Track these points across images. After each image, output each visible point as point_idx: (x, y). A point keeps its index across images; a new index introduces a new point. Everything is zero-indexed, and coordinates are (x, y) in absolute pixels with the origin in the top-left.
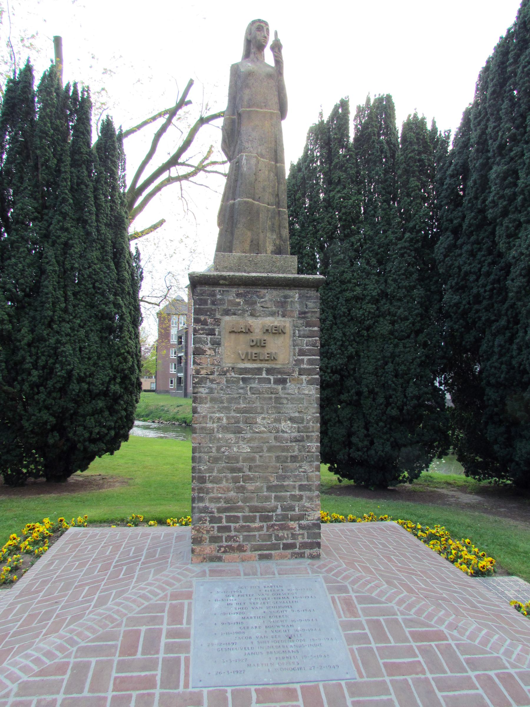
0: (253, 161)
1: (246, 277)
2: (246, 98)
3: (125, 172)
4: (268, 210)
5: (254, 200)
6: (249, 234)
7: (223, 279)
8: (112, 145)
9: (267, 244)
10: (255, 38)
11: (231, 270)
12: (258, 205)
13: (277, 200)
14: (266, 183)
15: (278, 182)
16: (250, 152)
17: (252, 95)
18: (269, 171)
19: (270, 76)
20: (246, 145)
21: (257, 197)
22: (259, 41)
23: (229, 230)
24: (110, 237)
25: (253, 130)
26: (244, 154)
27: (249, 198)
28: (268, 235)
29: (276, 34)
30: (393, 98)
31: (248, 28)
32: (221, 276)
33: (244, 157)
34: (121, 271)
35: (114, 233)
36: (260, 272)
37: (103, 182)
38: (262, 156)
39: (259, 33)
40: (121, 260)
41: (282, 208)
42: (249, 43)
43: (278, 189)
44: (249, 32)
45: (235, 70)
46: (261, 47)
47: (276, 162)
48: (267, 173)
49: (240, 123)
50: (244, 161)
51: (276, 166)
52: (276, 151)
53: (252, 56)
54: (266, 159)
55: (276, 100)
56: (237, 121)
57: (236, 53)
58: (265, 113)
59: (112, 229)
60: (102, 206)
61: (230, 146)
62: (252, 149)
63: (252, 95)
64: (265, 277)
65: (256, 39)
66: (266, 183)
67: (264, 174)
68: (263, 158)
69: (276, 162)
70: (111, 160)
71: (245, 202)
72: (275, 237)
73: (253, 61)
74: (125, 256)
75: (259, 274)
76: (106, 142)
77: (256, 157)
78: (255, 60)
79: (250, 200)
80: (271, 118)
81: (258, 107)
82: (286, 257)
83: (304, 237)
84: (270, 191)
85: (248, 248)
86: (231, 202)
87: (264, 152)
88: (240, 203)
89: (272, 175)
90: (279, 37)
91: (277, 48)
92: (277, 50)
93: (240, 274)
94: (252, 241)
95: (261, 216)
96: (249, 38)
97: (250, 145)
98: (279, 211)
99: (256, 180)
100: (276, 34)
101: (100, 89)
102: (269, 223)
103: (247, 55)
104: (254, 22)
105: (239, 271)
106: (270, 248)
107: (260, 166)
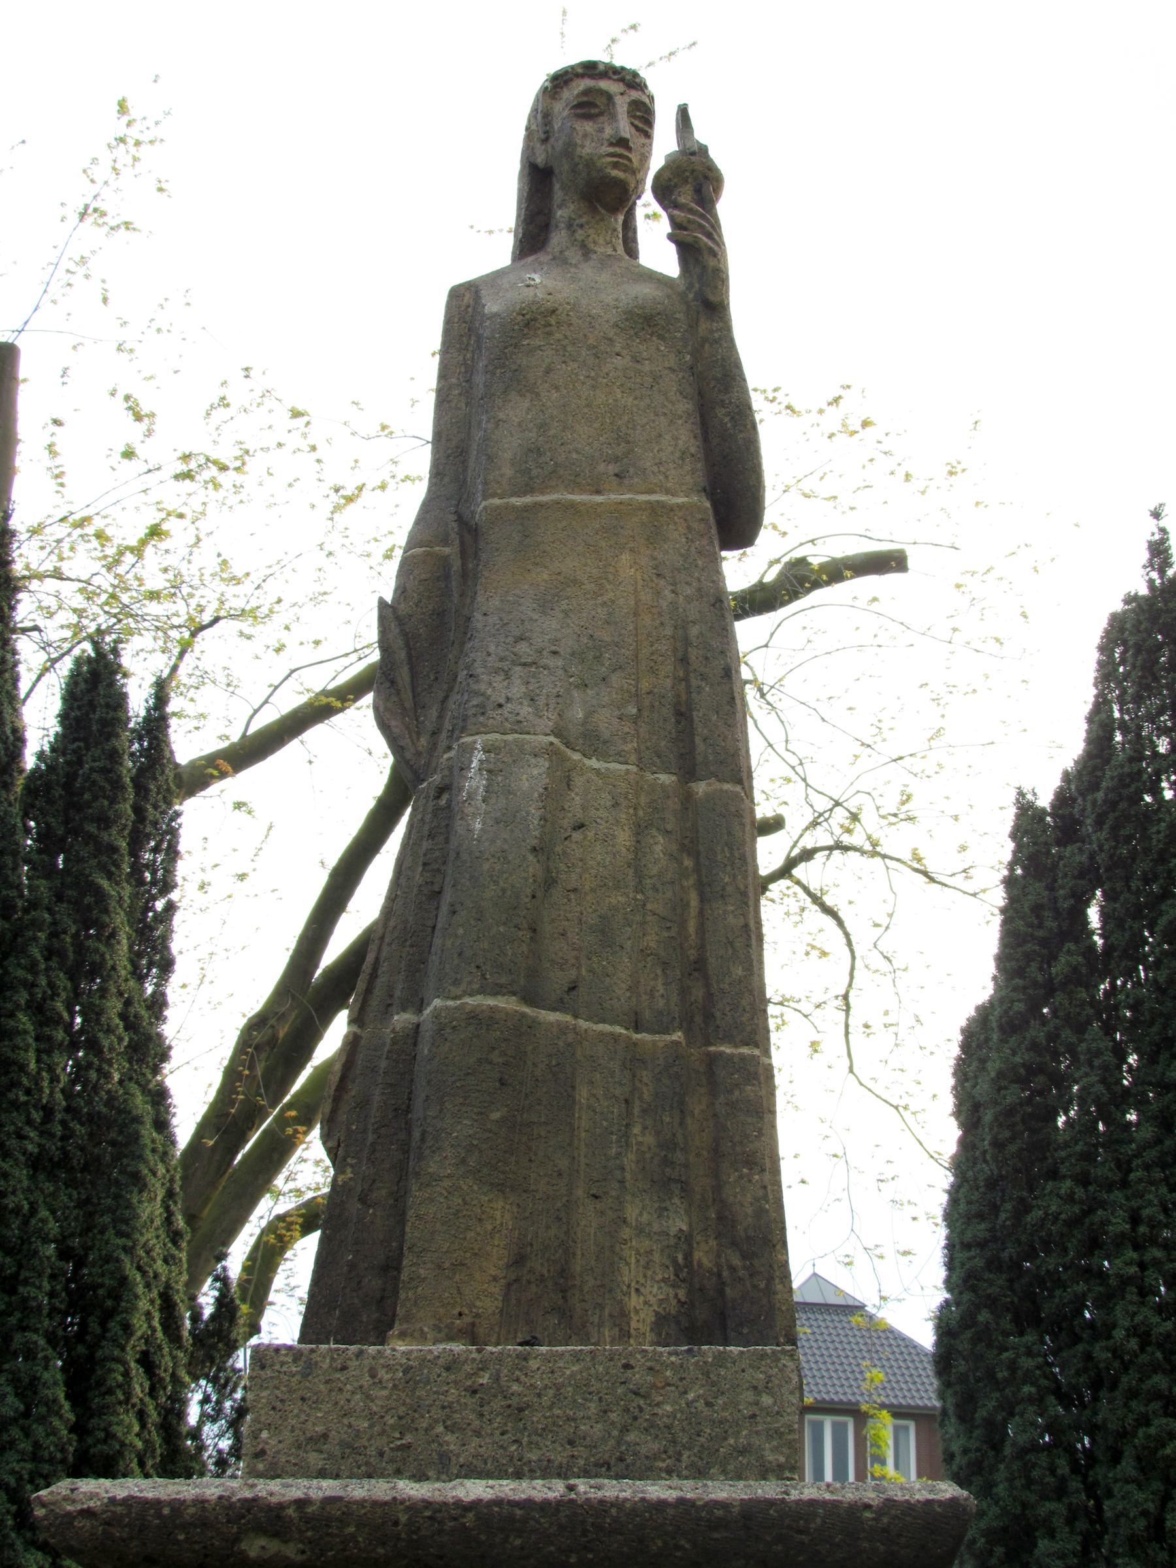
0: (532, 776)
1: (416, 1508)
2: (509, 445)
3: (174, 896)
4: (634, 1059)
5: (530, 999)
6: (501, 1211)
7: (260, 1529)
8: (105, 771)
9: (628, 1274)
10: (569, 151)
11: (352, 1459)
12: (563, 1029)
13: (698, 993)
14: (617, 899)
15: (701, 886)
16: (519, 726)
17: (543, 427)
18: (639, 830)
19: (644, 322)
20: (496, 688)
21: (558, 980)
22: (590, 163)
23: (381, 1193)
24: (53, 1227)
25: (545, 605)
26: (480, 741)
27: (497, 990)
28: (631, 1212)
29: (683, 114)
30: (712, 154)
31: (535, 110)
32: (251, 1504)
33: (478, 756)
34: (103, 1410)
35: (80, 1204)
36: (547, 1471)
37: (36, 952)
38: (593, 743)
39: (588, 126)
40: (107, 1349)
41: (728, 1039)
42: (538, 180)
43: (701, 929)
44: (541, 126)
45: (469, 319)
46: (610, 197)
47: (689, 771)
48: (624, 837)
49: (469, 577)
50: (474, 781)
51: (688, 798)
52: (683, 714)
53: (558, 238)
54: (621, 757)
55: (685, 437)
56: (456, 565)
57: (481, 235)
58: (620, 511)
59: (71, 1183)
60: (22, 1068)
61: (419, 705)
62: (526, 710)
63: (543, 427)
64: (545, 1506)
65: (589, 151)
66: (617, 899)
67: (606, 843)
68: (603, 756)
69: (689, 771)
70: (90, 838)
71: (474, 1017)
72: (678, 1223)
73: (561, 260)
74: (127, 1328)
75: (507, 1489)
76: (80, 763)
77: (551, 752)
78: (574, 255)
79: (507, 1004)
80: (654, 536)
81: (575, 484)
82: (721, 1359)
83: (1109, 1186)
84: (651, 941)
85: (490, 1305)
86: (402, 1019)
87: (605, 721)
88: (443, 1026)
89: (659, 845)
90: (701, 134)
91: (693, 185)
92: (685, 196)
93: (379, 1489)
94: (519, 1260)
95: (583, 1094)
96: (540, 160)
97: (517, 690)
98: (712, 1061)
99: (550, 882)
100: (683, 114)
101: (142, 532)
102: (643, 1137)
103: (534, 234)
104: (560, 81)
105: (403, 1463)
106: (647, 1296)
107: (575, 800)
